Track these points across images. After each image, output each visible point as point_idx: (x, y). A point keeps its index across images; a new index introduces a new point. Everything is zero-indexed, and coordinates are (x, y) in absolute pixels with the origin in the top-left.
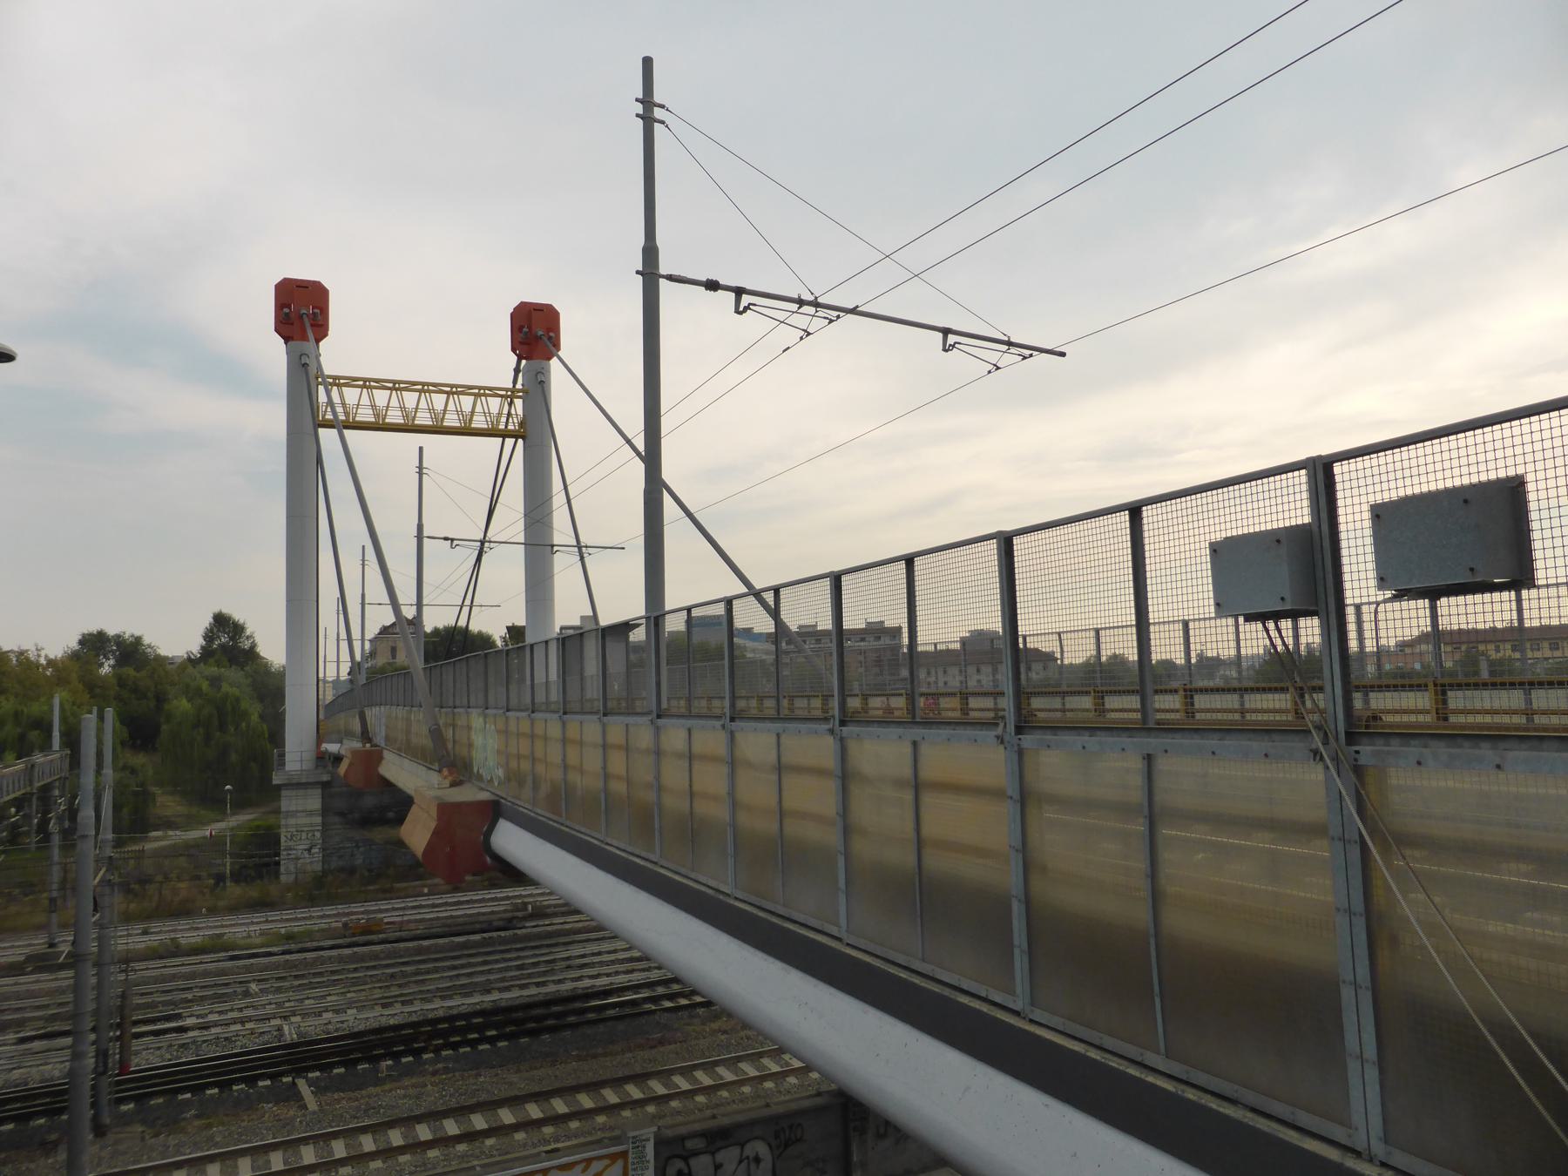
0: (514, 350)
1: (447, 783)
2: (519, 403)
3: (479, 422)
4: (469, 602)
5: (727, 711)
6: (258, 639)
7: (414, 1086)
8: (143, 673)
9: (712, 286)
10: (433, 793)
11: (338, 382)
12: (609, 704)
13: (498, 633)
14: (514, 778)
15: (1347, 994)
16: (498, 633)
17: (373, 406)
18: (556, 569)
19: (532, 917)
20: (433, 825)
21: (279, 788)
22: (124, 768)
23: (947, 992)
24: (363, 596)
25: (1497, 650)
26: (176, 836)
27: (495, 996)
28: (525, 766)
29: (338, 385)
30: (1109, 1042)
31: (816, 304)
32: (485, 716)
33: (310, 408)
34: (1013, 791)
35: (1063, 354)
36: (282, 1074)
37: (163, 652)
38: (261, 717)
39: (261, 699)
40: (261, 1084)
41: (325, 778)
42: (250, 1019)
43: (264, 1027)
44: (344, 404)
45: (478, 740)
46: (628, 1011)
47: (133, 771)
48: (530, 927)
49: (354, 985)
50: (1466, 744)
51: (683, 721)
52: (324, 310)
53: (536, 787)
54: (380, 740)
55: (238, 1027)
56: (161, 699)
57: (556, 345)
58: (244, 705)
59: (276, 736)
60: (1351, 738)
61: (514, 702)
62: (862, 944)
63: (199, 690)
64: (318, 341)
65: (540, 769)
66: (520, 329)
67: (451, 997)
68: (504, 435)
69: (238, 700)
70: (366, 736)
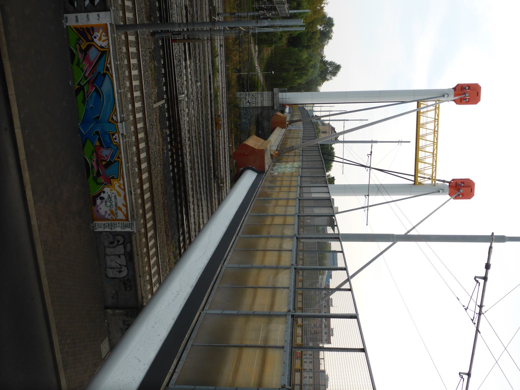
0: (453, 180)
1: (272, 153)
2: (430, 182)
3: (421, 166)
8: (317, 41)
9: (488, 266)
10: (269, 147)
11: (437, 108)
12: (302, 218)
13: (332, 173)
14: (274, 179)
16: (332, 173)
17: (427, 123)
20: (256, 148)
23: (179, 355)
26: (255, 55)
28: (278, 184)
29: (435, 109)
31: (480, 314)
32: (299, 168)
38: (300, 84)
39: (306, 83)
40: (164, 87)
41: (275, 108)
42: (187, 83)
45: (289, 165)
46: (180, 222)
47: (280, 39)
48: (214, 185)
49: (197, 120)
51: (293, 284)
52: (468, 102)
53: (270, 187)
54: (290, 127)
55: (185, 79)
56: (308, 47)
57: (456, 198)
58: (305, 77)
59: (292, 89)
62: (201, 319)
63: (310, 61)
65: (277, 189)
67: (190, 155)
69: (307, 75)
70: (291, 122)
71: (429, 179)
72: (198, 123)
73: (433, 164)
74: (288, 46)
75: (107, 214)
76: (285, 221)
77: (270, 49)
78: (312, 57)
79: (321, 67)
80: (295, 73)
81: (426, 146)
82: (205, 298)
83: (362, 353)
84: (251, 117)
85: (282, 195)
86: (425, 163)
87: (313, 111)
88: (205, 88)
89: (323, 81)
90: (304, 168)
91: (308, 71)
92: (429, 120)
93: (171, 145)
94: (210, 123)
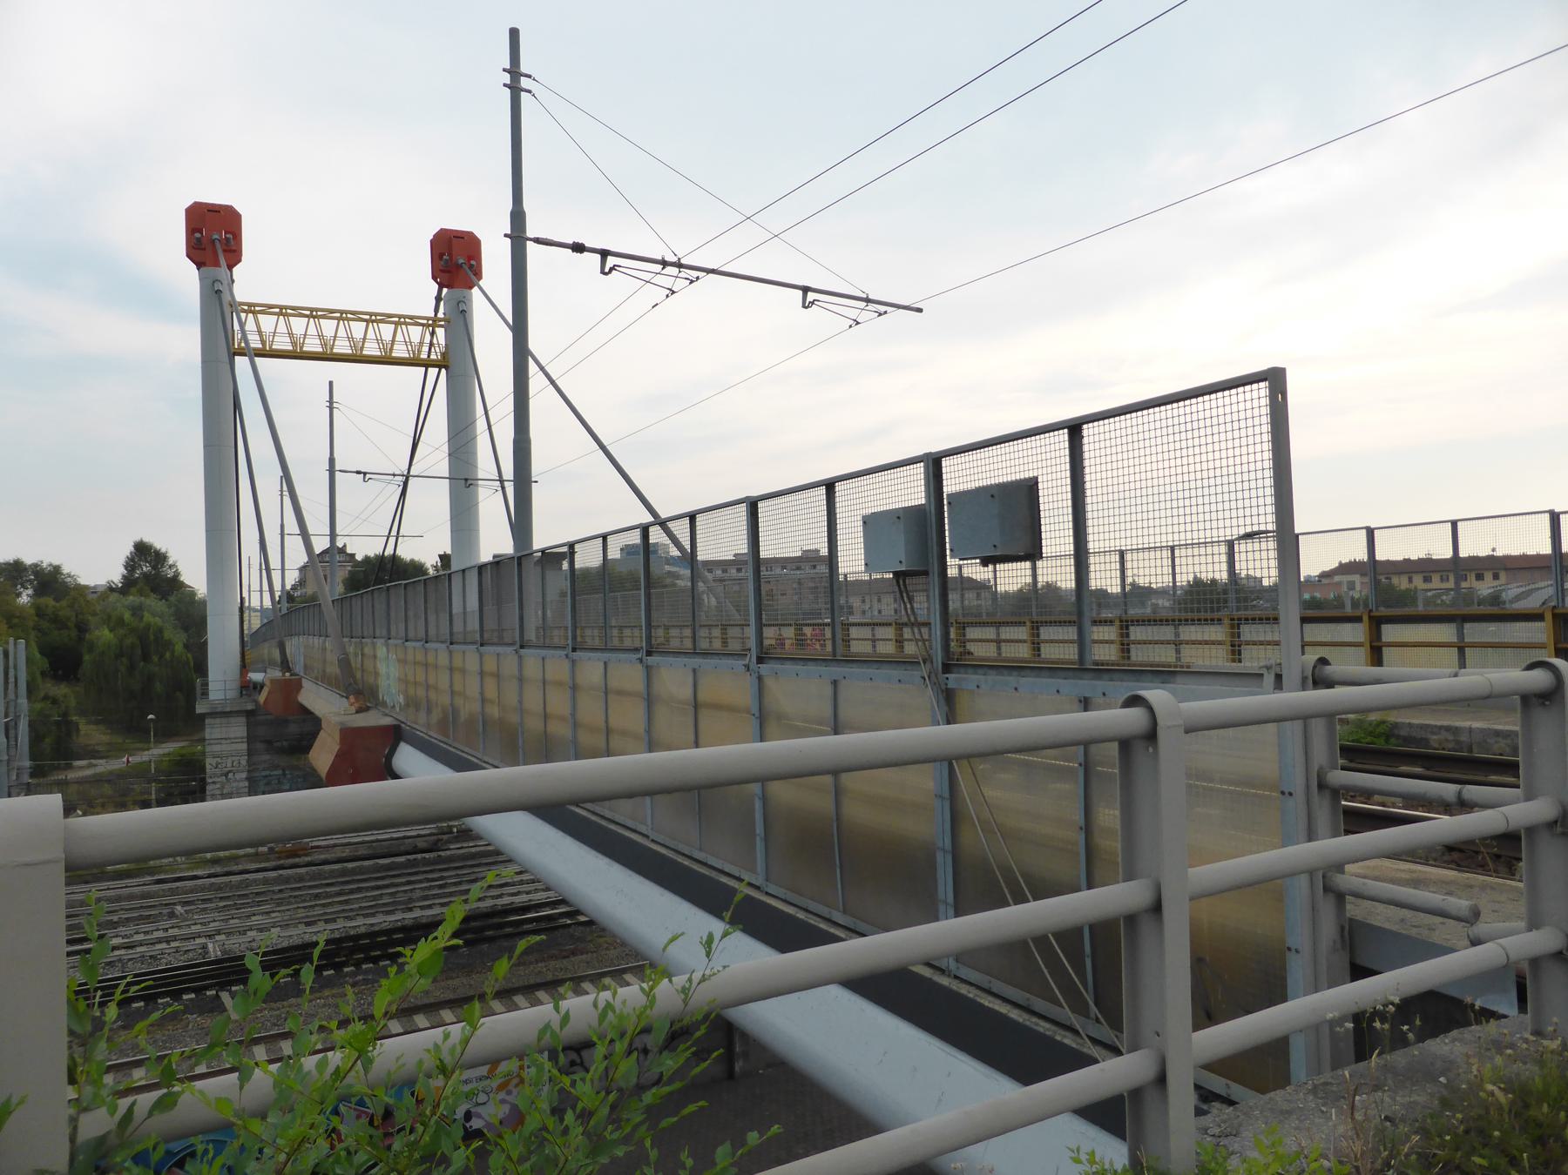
0: (434, 278)
1: (353, 709)
2: (440, 332)
3: (400, 351)
4: (395, 530)
5: (752, 643)
6: (181, 568)
7: (333, 996)
8: (64, 603)
9: (578, 248)
10: (337, 719)
11: (252, 309)
13: (430, 560)
14: (412, 703)
15: (940, 857)
16: (430, 560)
17: (291, 334)
18: (481, 498)
19: (457, 839)
20: (337, 748)
21: (203, 717)
22: (46, 698)
23: (714, 874)
24: (282, 526)
25: (1410, 580)
26: (103, 766)
27: (417, 913)
28: (421, 693)
29: (254, 313)
30: (813, 906)
31: (679, 265)
32: (387, 646)
33: (224, 336)
34: (755, 710)
35: (920, 310)
36: (207, 988)
37: (83, 581)
38: (186, 646)
39: (186, 629)
40: (185, 997)
41: (250, 707)
42: (175, 938)
43: (189, 945)
44: (260, 332)
47: (55, 701)
48: (455, 849)
49: (279, 905)
50: (993, 672)
51: (599, 654)
52: (237, 235)
53: (429, 711)
55: (164, 945)
56: (82, 628)
57: (478, 274)
58: (167, 635)
59: (201, 668)
60: (947, 668)
61: (411, 635)
63: (121, 622)
64: (230, 267)
65: (432, 695)
66: (441, 256)
67: (373, 915)
68: (427, 364)
69: (161, 630)
70: (285, 665)
71: (433, 334)
72: (290, 903)
73: (396, 323)
74: (78, 680)
75: (508, 1098)
76: (492, 674)
77: (83, 728)
78: (109, 617)
79: (141, 593)
80: (155, 659)
81: (350, 338)
82: (627, 834)
83: (1085, 433)
84: (276, 767)
85: (443, 680)
86: (393, 341)
87: (262, 610)
88: (192, 892)
89: (182, 585)
90: (389, 631)
91: (148, 627)
92: (282, 328)
93: (345, 964)
94: (289, 872)
